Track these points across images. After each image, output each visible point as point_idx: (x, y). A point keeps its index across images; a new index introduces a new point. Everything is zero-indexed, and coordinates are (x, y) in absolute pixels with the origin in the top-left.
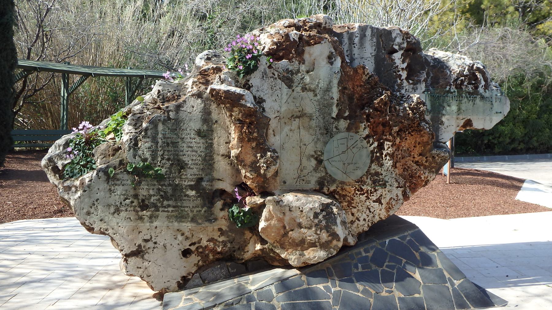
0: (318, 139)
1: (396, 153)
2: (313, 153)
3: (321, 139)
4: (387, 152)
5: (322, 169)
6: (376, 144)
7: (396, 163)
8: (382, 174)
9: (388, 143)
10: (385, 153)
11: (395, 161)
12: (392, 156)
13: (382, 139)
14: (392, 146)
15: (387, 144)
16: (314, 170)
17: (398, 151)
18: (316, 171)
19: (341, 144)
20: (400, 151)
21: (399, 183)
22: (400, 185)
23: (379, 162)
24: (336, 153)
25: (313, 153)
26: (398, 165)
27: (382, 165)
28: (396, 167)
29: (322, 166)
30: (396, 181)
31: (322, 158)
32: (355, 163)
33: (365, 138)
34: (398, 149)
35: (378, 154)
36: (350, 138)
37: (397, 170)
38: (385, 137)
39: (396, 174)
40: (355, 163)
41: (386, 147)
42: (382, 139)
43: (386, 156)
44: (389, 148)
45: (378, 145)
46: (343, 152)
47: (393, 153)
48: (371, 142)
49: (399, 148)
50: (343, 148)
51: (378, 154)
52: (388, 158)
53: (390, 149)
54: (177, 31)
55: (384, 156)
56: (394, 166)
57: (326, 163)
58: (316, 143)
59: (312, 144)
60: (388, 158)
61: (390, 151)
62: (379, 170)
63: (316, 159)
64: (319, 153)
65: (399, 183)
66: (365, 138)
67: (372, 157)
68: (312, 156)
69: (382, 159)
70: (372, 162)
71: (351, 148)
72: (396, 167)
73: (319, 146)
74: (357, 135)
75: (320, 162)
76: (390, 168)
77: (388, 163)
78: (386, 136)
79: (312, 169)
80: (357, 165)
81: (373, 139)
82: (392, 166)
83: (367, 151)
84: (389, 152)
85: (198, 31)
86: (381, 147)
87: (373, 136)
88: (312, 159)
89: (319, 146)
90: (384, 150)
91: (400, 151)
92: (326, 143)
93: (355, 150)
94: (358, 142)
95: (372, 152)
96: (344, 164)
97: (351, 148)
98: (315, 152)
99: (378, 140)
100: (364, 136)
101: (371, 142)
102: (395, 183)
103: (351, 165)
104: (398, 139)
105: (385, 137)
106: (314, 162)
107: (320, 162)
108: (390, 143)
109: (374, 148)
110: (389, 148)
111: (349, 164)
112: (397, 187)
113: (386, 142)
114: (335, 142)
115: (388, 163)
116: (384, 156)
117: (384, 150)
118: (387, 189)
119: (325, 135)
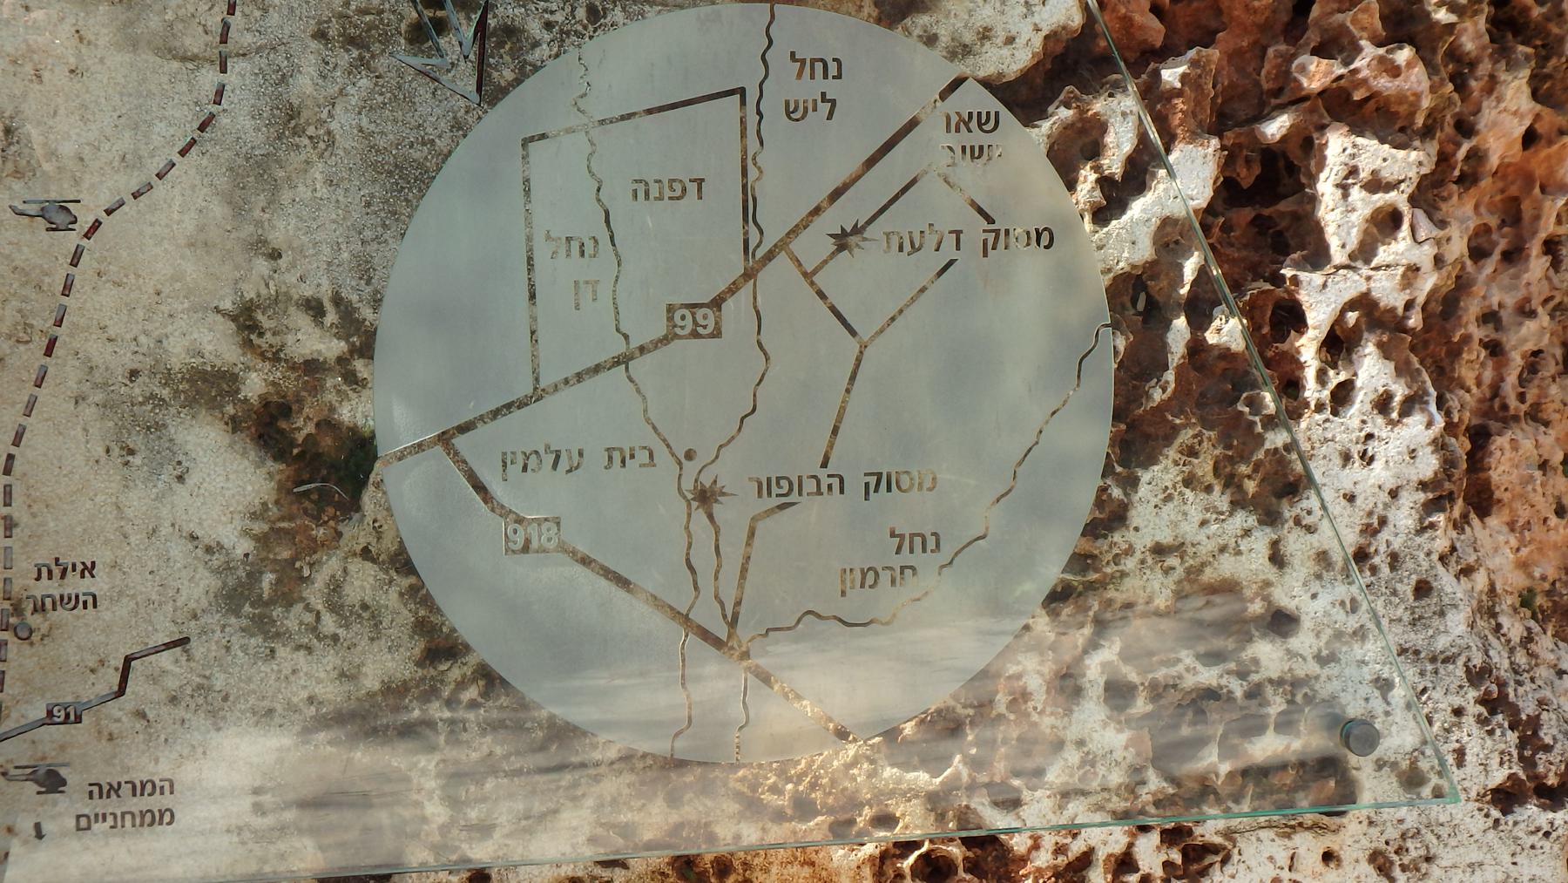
0: (289, 121)
1: (1493, 289)
2: (217, 344)
3: (343, 122)
4: (1349, 286)
5: (363, 582)
6: (1190, 176)
7: (1480, 438)
8: (1281, 622)
9: (1374, 154)
10: (1321, 300)
11: (1466, 403)
12: (1429, 341)
13: (1284, 94)
14: (1428, 195)
15: (1352, 176)
16: (235, 597)
17: (1514, 256)
18: (262, 625)
19: (642, 190)
20: (1537, 264)
21: (1530, 738)
22: (1550, 770)
23: (1239, 438)
24: (573, 334)
25: (217, 344)
26: (1508, 461)
27: (1282, 488)
28: (1482, 501)
29: (355, 534)
30: (1493, 704)
31: (352, 412)
32: (880, 482)
33: (1025, 96)
34: (1506, 237)
35: (1227, 331)
36: (786, 85)
37: (1492, 541)
38: (1316, 74)
39: (1487, 609)
40: (880, 482)
41: (1339, 216)
42: (1284, 94)
43: (1338, 345)
44: (1388, 222)
45: (1228, 191)
46: (696, 319)
47: (1445, 306)
48: (1119, 144)
49: (1513, 214)
50: (691, 248)
51: (1227, 331)
52: (1372, 370)
53: (1397, 250)
54: (1205, 790)
55: (1307, 348)
56: (1464, 488)
57: (405, 492)
58: (256, 177)
59: (191, 200)
60: (1372, 370)
61: (1404, 268)
62: (1251, 562)
63: (267, 427)
64: (315, 341)
65: (1530, 738)
66: (1025, 96)
67: (1138, 369)
68: (207, 387)
69: (1290, 386)
70: (1135, 440)
71: (814, 245)
72: (1482, 501)
73: (316, 224)
74: (901, 45)
75: (325, 471)
76: (1404, 517)
77: (1370, 449)
78: (1335, 45)
79: (199, 586)
80: (906, 511)
81: (1153, 95)
82: (1436, 496)
83: (1066, 280)
84: (1387, 290)
85: (309, 90)
86: (1264, 210)
87: (1147, 58)
88: (205, 441)
89: (316, 224)
90: (1317, 257)
91: (1537, 264)
92: (405, 179)
93: (864, 279)
94: (934, 145)
95: (1138, 298)
96: (705, 497)
97: (814, 245)
98: (246, 320)
99: (1227, 116)
100: (1015, 60)
101: (1119, 144)
102: (1471, 736)
103: (812, 513)
104: (1516, 93)
105: (1316, 74)
106: (225, 485)
107: (325, 471)
108: (1406, 163)
109: (1170, 237)
110: (1388, 222)
111: (781, 492)
112: (1505, 798)
113: (1337, 144)
114: (559, 171)
115: (1370, 449)
116: (1307, 348)
117: (1317, 257)
118: (1353, 837)
119: (398, 58)
